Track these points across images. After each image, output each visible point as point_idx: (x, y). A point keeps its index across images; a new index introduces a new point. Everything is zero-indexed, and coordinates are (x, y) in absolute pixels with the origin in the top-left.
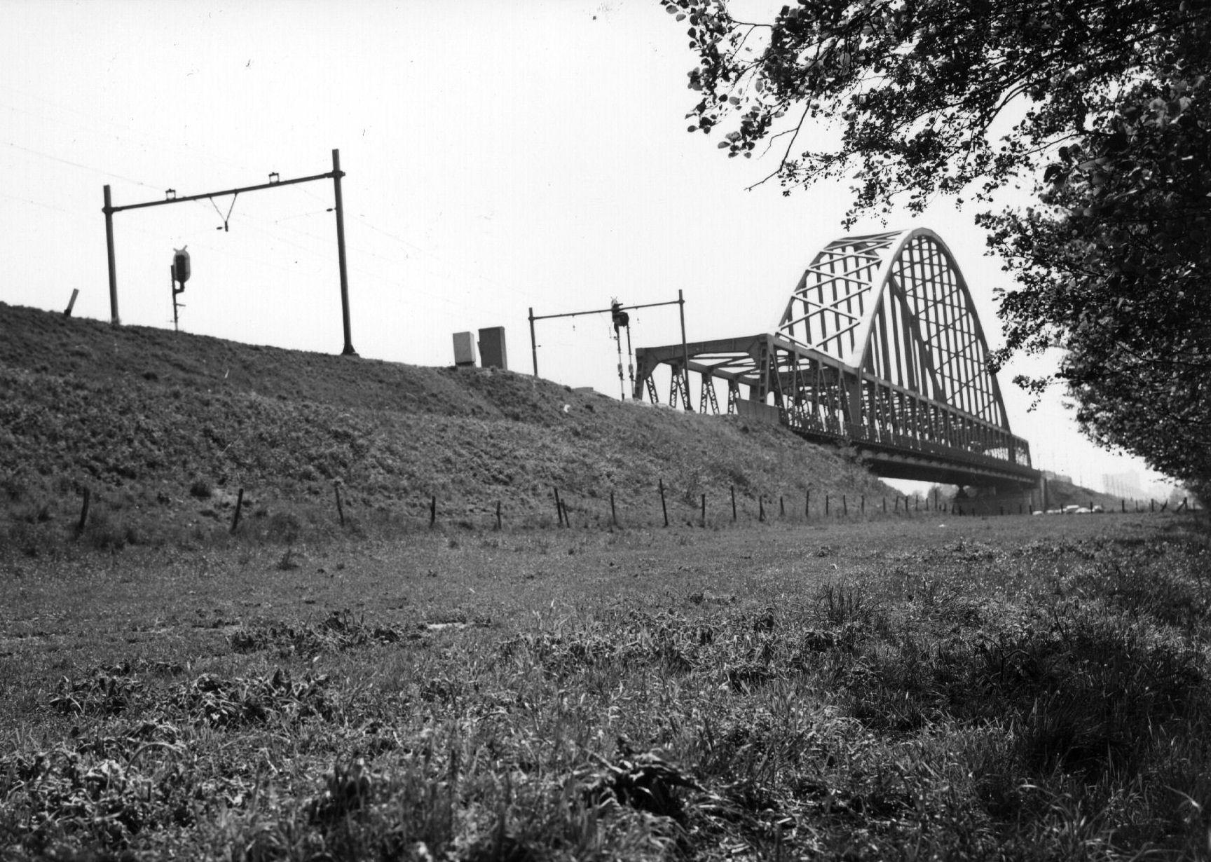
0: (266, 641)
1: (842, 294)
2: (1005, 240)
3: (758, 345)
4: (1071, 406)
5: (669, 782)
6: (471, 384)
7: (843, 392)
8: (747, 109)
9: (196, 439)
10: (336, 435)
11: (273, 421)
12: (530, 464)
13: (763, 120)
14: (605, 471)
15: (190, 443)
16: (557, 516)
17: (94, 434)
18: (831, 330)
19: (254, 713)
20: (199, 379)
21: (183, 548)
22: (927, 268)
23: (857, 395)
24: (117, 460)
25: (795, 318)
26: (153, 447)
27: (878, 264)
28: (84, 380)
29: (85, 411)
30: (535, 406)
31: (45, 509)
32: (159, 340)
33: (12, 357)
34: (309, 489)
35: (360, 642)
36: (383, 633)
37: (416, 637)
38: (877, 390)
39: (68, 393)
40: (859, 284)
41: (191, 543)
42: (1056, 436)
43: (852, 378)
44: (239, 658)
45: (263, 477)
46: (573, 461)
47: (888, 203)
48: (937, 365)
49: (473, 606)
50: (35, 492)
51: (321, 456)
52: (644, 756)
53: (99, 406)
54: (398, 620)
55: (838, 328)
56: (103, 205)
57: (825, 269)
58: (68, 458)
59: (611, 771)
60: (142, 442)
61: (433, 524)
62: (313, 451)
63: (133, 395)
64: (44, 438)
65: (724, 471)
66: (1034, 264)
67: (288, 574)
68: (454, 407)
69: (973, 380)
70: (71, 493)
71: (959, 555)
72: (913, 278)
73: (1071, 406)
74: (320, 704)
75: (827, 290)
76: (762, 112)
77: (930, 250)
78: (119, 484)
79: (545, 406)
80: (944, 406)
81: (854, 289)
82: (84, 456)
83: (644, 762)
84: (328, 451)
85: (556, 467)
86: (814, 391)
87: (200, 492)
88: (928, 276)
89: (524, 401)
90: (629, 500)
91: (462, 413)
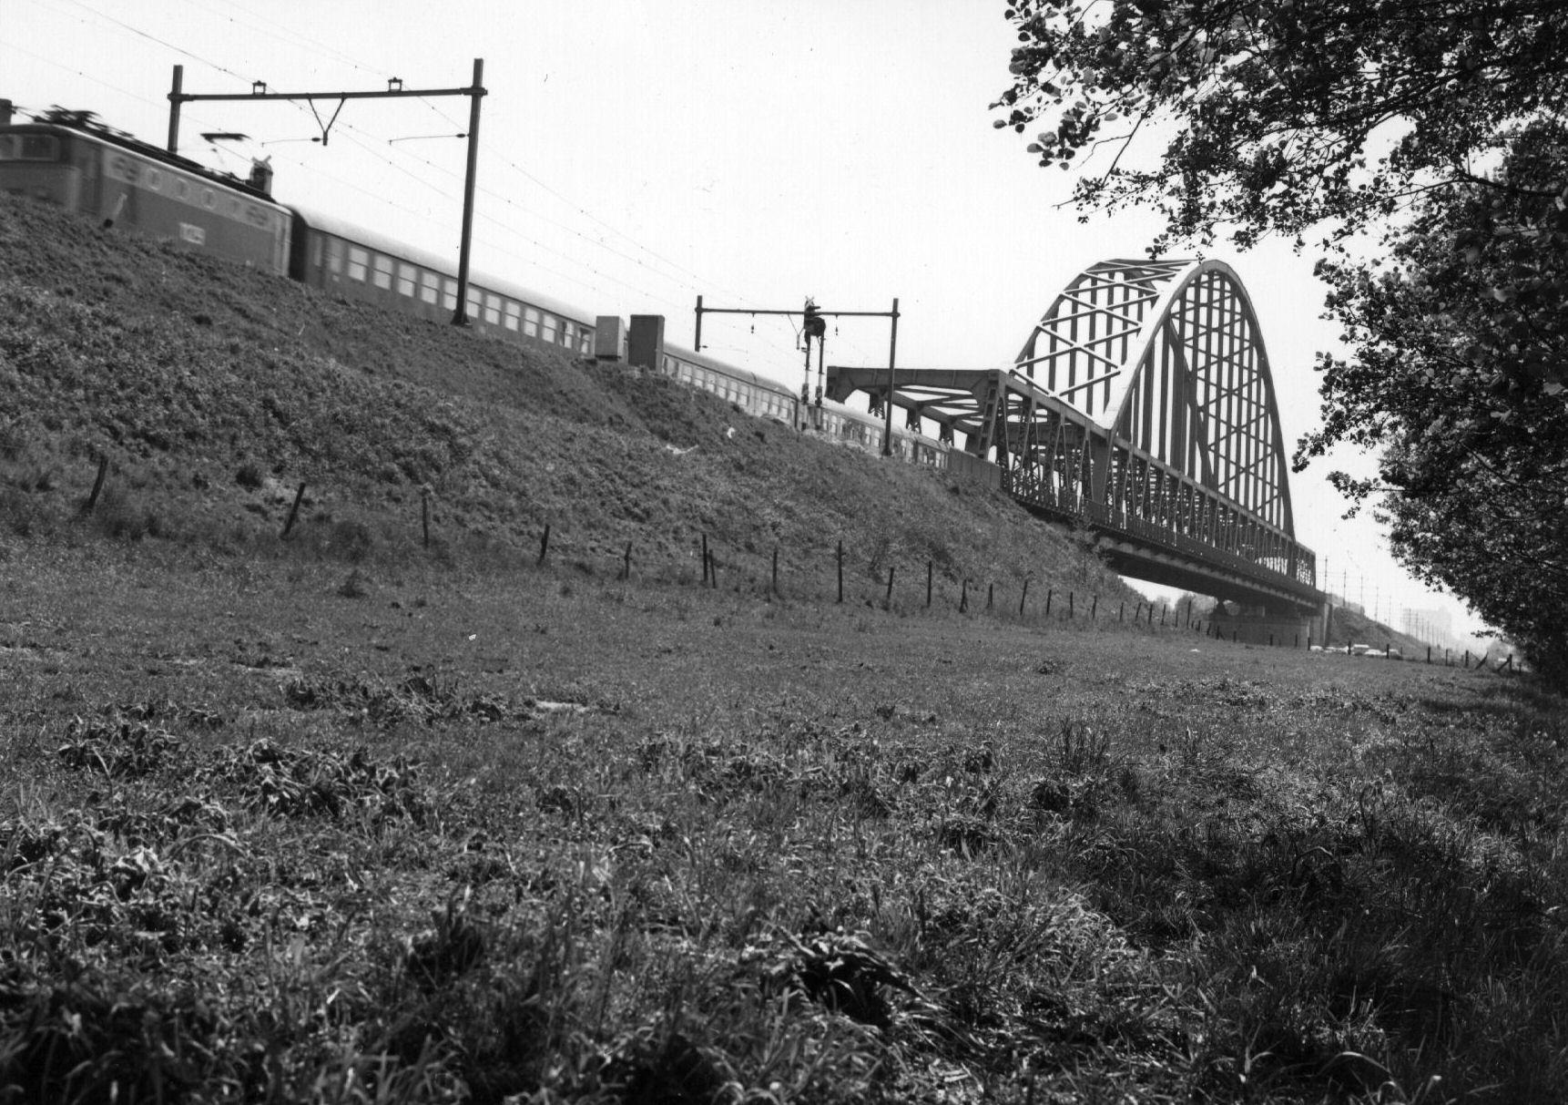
0: (329, 699)
1: (1101, 333)
2: (1350, 302)
3: (986, 383)
4: (1386, 519)
5: (874, 977)
6: (613, 386)
7: (1086, 458)
8: (1069, 103)
9: (252, 409)
10: (432, 429)
11: (354, 400)
12: (675, 499)
13: (1089, 121)
14: (769, 520)
15: (244, 414)
16: (700, 571)
17: (122, 386)
18: (1082, 378)
19: (325, 801)
20: (265, 333)
21: (218, 549)
22: (1216, 313)
23: (1103, 465)
24: (148, 423)
25: (1038, 355)
26: (196, 413)
27: (1154, 301)
28: (118, 314)
29: (115, 355)
30: (690, 424)
31: (47, 475)
32: (220, 274)
33: (29, 270)
34: (389, 494)
35: (453, 715)
36: (483, 707)
37: (523, 717)
38: (1130, 461)
39: (96, 328)
40: (1126, 323)
41: (229, 546)
42: (1354, 551)
43: (1100, 441)
44: (297, 716)
45: (332, 471)
46: (730, 503)
47: (1210, 234)
48: (1211, 439)
49: (595, 682)
50: (36, 451)
51: (409, 453)
52: (846, 939)
53: (133, 351)
54: (494, 690)
55: (1091, 374)
56: (169, 90)
57: (1085, 297)
58: (85, 412)
59: (800, 953)
60: (182, 405)
61: (541, 562)
62: (399, 445)
63: (179, 342)
64: (57, 382)
65: (922, 540)
66: (1382, 338)
67: (353, 604)
68: (587, 412)
69: (1256, 465)
70: (83, 459)
71: (1222, 695)
72: (1196, 324)
73: (1386, 519)
74: (409, 800)
75: (1083, 324)
76: (1088, 111)
77: (1222, 290)
78: (145, 454)
79: (703, 427)
80: (1212, 494)
81: (1117, 327)
82: (106, 412)
83: (845, 948)
84: (419, 448)
85: (708, 507)
86: (1049, 452)
87: (248, 479)
88: (1215, 324)
89: (678, 416)
90: (797, 562)
91: (597, 421)
